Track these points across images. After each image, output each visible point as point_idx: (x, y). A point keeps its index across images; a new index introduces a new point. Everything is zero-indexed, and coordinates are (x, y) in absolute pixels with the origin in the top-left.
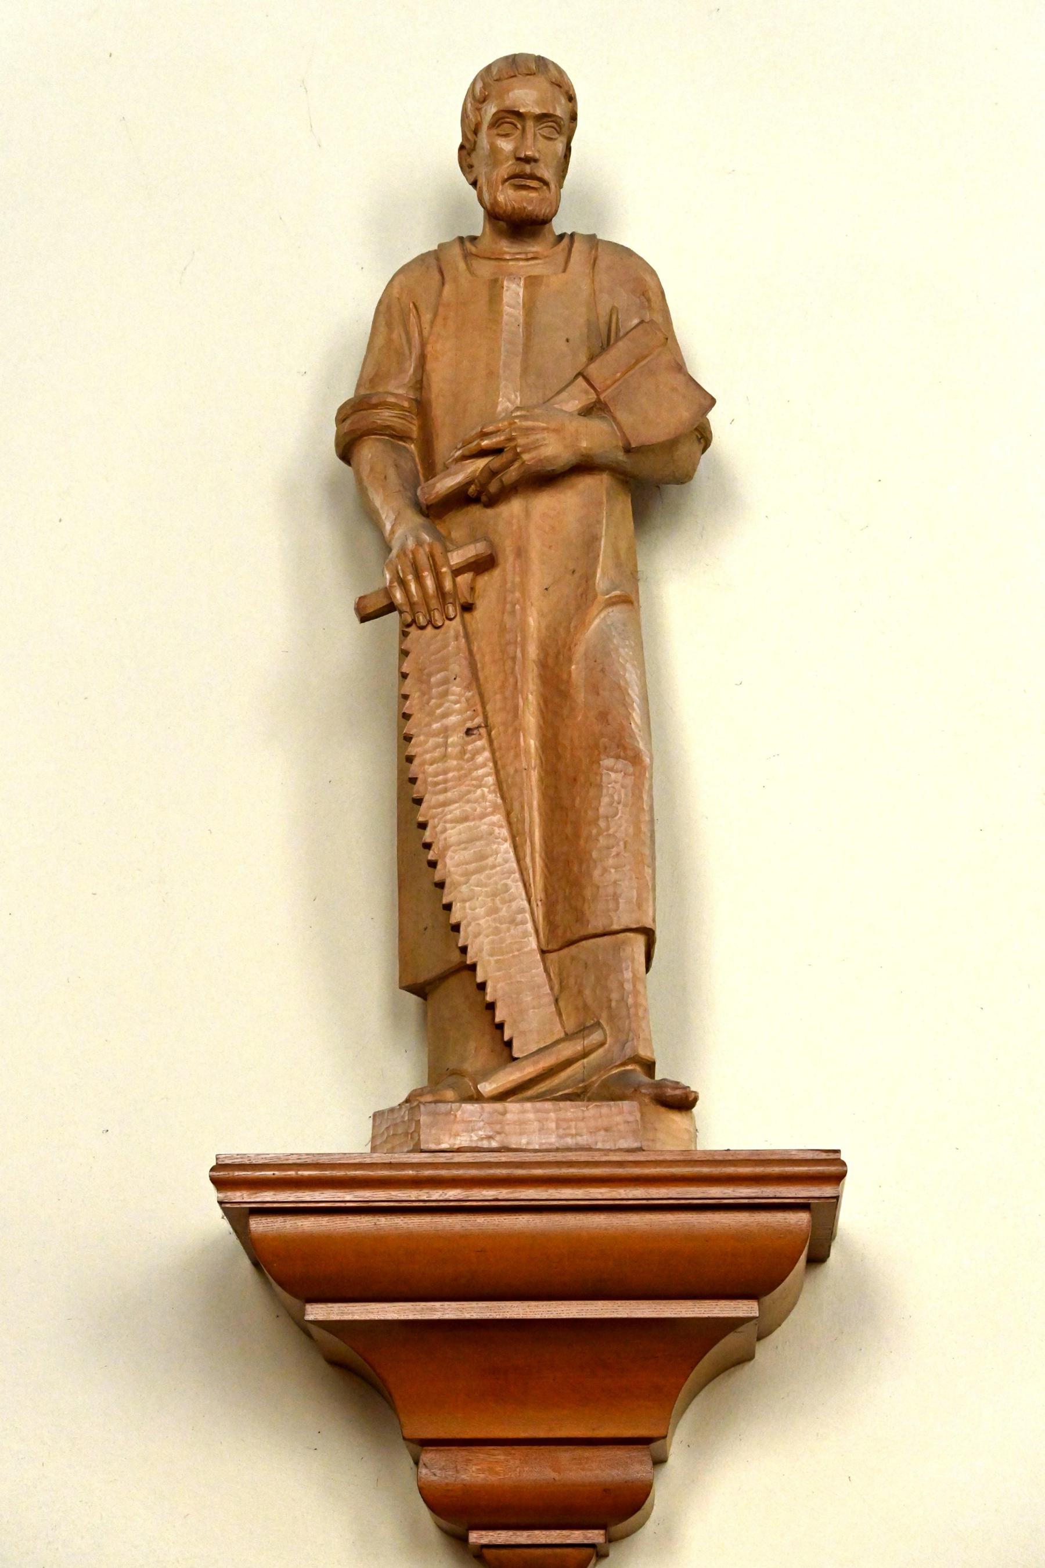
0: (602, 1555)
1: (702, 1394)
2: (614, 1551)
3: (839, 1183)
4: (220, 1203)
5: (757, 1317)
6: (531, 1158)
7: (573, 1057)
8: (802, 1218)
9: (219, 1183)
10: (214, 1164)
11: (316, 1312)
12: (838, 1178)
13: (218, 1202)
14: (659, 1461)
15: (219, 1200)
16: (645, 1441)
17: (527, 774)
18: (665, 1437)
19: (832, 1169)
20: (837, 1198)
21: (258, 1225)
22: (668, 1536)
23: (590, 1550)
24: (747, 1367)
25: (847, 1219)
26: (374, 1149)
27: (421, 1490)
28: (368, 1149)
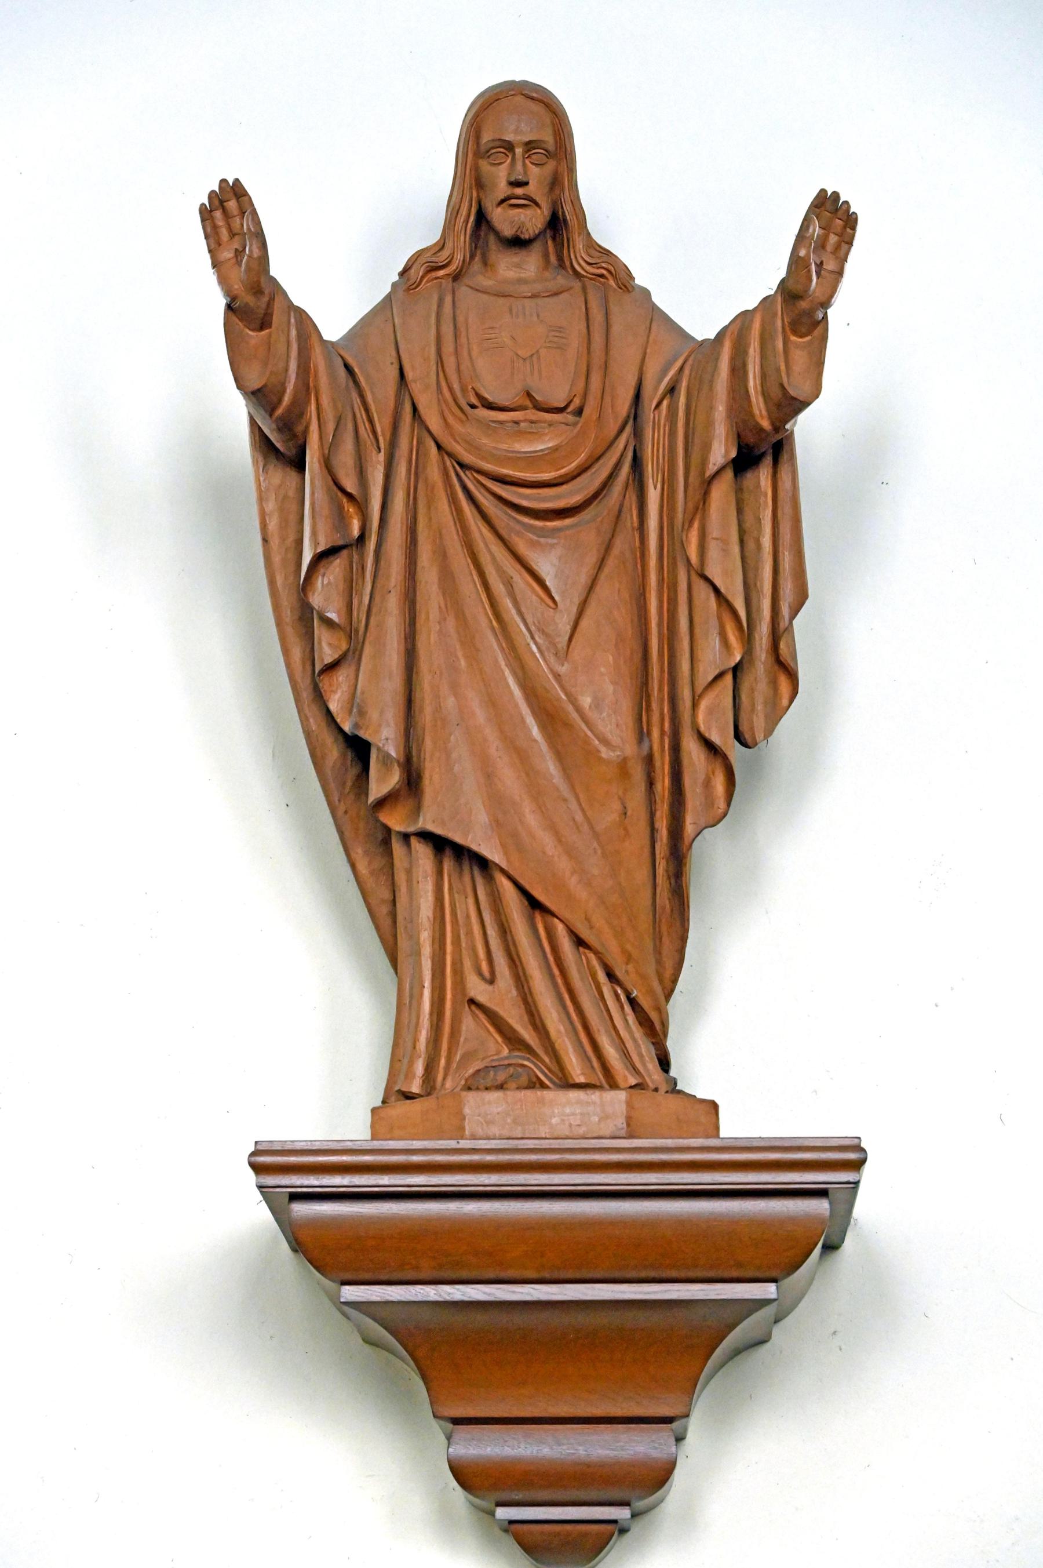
0: (623, 1531)
1: (720, 1373)
2: (636, 1529)
3: (860, 1169)
4: (260, 1187)
5: (775, 1300)
6: (386, 1295)
7: (555, 1161)
8: (820, 1206)
9: (258, 1169)
10: (253, 1149)
11: (350, 1293)
12: (858, 1165)
13: (257, 1186)
14: (679, 1439)
15: (258, 1184)
16: (668, 1420)
17: (558, 1076)
18: (687, 1416)
19: (852, 1156)
20: (857, 1183)
21: (301, 1209)
22: (689, 1520)
23: (610, 1527)
24: (767, 1346)
25: (863, 1208)
26: (374, 1137)
27: (449, 1461)
28: (367, 1135)
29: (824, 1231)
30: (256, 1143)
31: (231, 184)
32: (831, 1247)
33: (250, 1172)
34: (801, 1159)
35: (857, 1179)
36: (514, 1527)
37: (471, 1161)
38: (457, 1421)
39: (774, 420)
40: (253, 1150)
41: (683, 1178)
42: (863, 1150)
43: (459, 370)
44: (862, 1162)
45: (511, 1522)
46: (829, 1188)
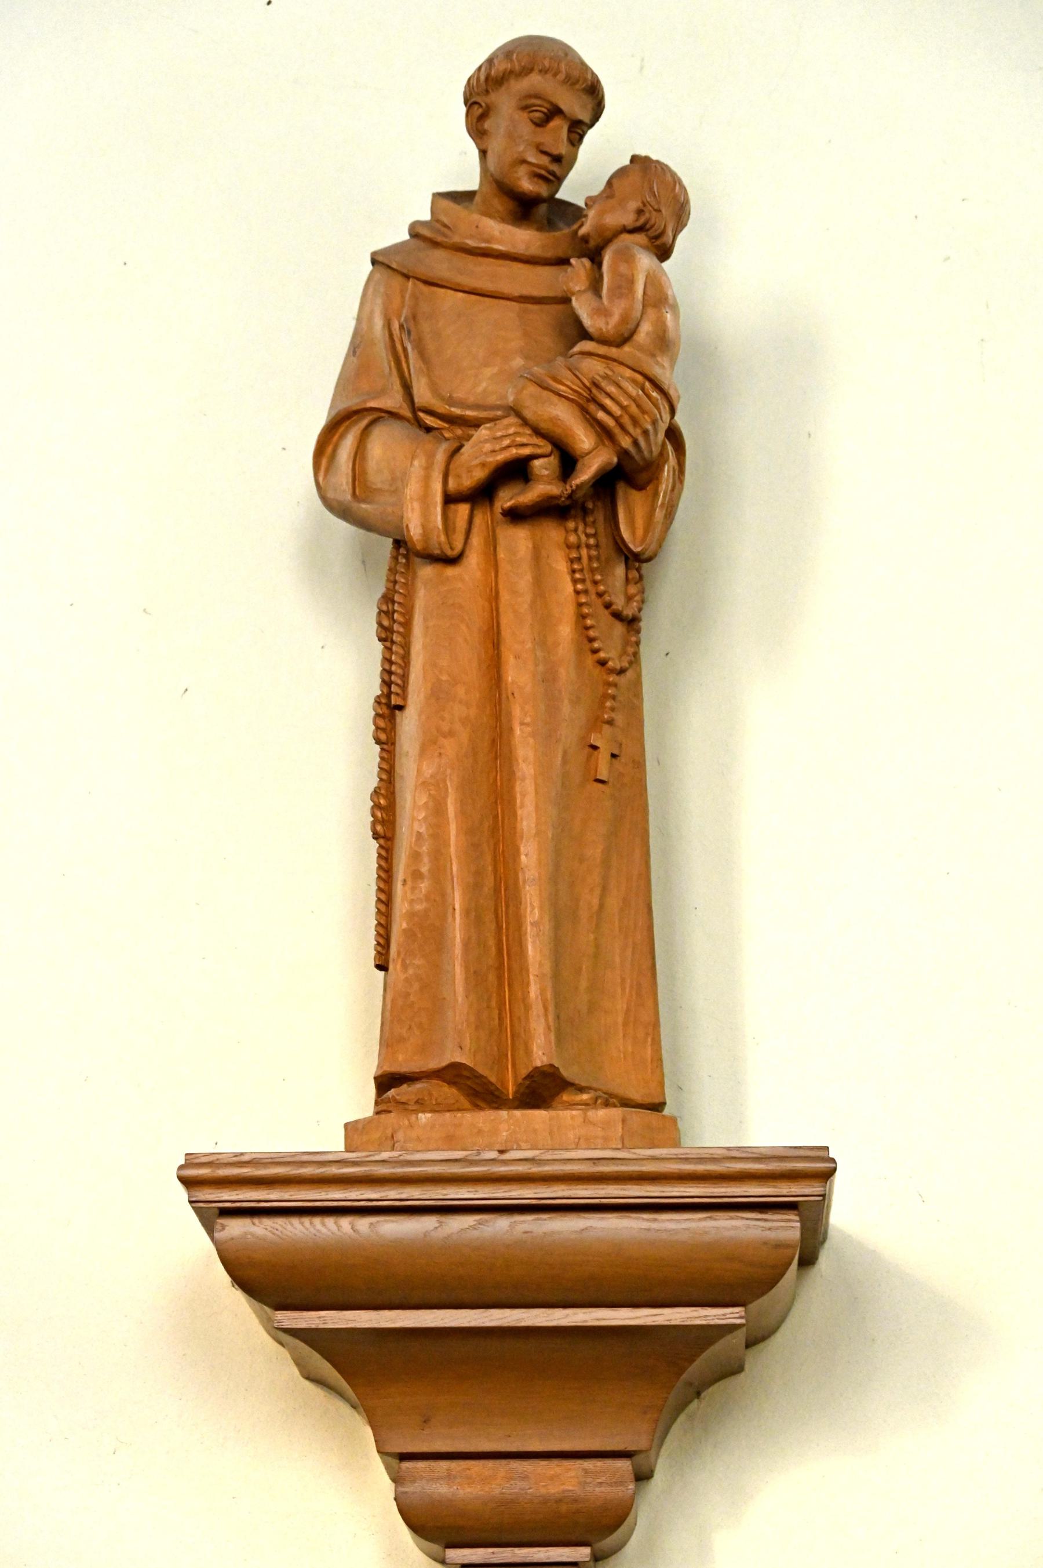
12: (827, 1175)
33: (181, 1193)
38: (404, 1457)
42: (833, 1161)
44: (835, 1170)
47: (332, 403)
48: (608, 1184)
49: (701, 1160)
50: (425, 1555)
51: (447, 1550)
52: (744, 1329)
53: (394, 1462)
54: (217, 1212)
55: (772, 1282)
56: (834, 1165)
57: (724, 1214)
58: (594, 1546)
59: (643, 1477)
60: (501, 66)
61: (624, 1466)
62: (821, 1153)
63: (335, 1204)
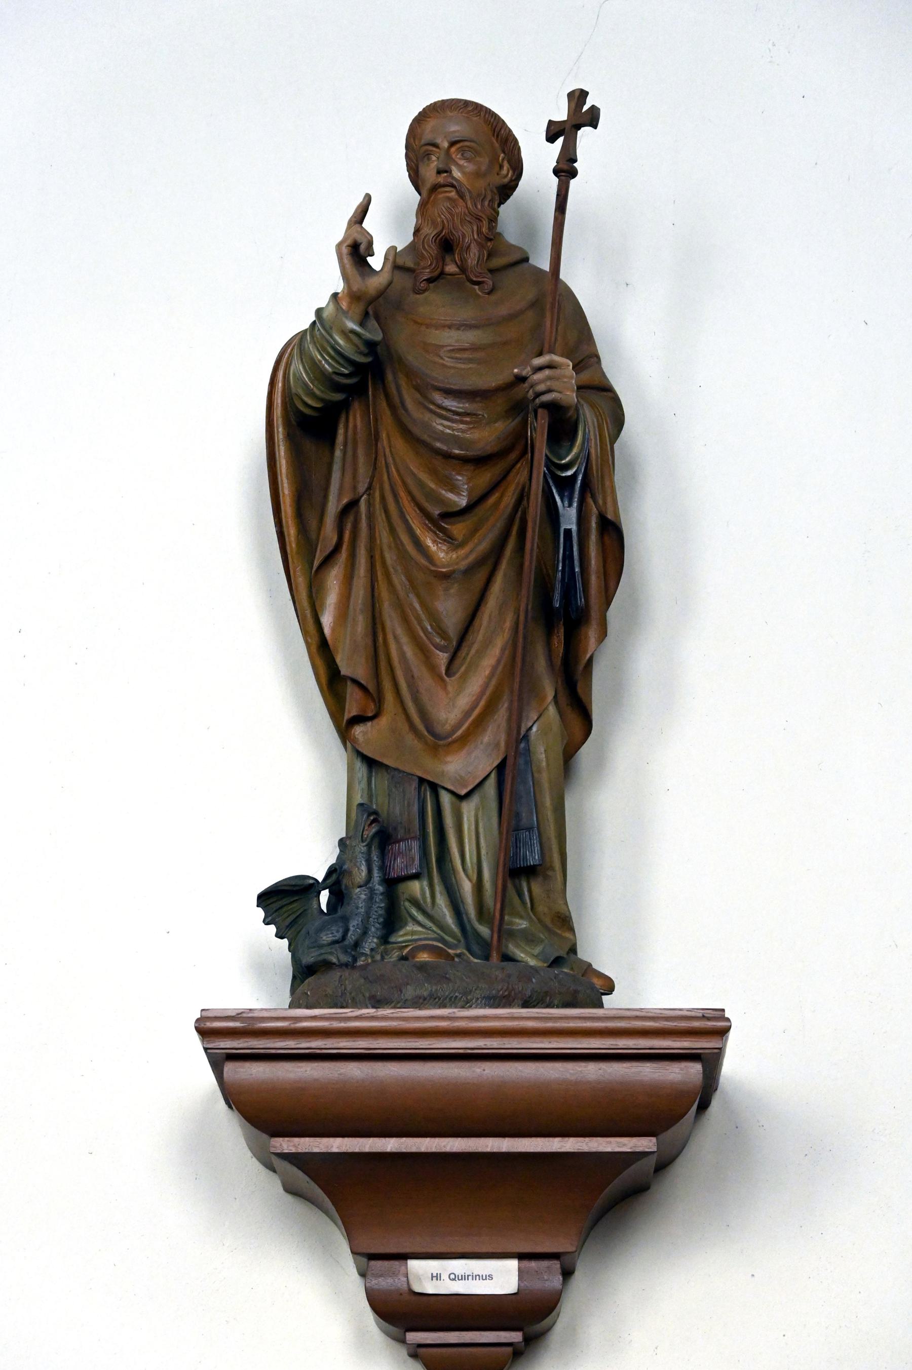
4: (206, 1049)
12: (723, 1032)
26: (291, 1006)
29: (228, 1099)
30: (202, 1010)
31: (397, 251)
32: (704, 1106)
33: (195, 1037)
34: (355, 1027)
35: (721, 1046)
36: (422, 1351)
37: (576, 1027)
38: (373, 1257)
39: (529, 380)
40: (199, 1016)
41: (359, 1045)
42: (728, 1020)
43: (598, 408)
44: (729, 1028)
45: (420, 1346)
46: (701, 1053)
47: (562, 121)
48: (522, 1037)
49: (637, 1018)
50: (389, 1339)
51: (407, 1334)
52: (656, 1155)
53: (364, 1260)
54: (225, 1056)
55: (675, 1118)
56: (729, 1024)
57: (345, 1063)
58: (525, 1330)
59: (567, 1274)
60: (321, 319)
61: (556, 1265)
62: (719, 1015)
63: (307, 1051)
